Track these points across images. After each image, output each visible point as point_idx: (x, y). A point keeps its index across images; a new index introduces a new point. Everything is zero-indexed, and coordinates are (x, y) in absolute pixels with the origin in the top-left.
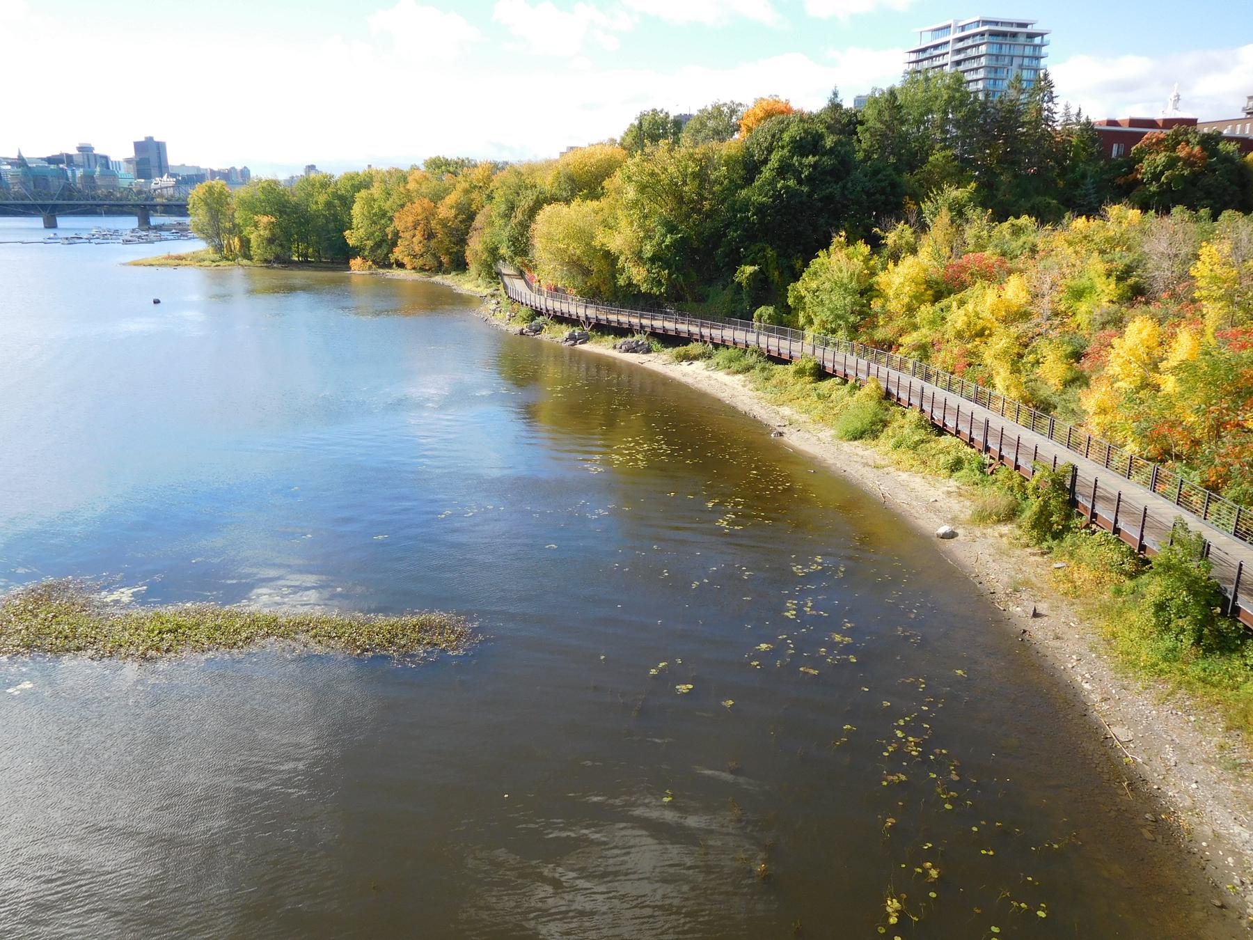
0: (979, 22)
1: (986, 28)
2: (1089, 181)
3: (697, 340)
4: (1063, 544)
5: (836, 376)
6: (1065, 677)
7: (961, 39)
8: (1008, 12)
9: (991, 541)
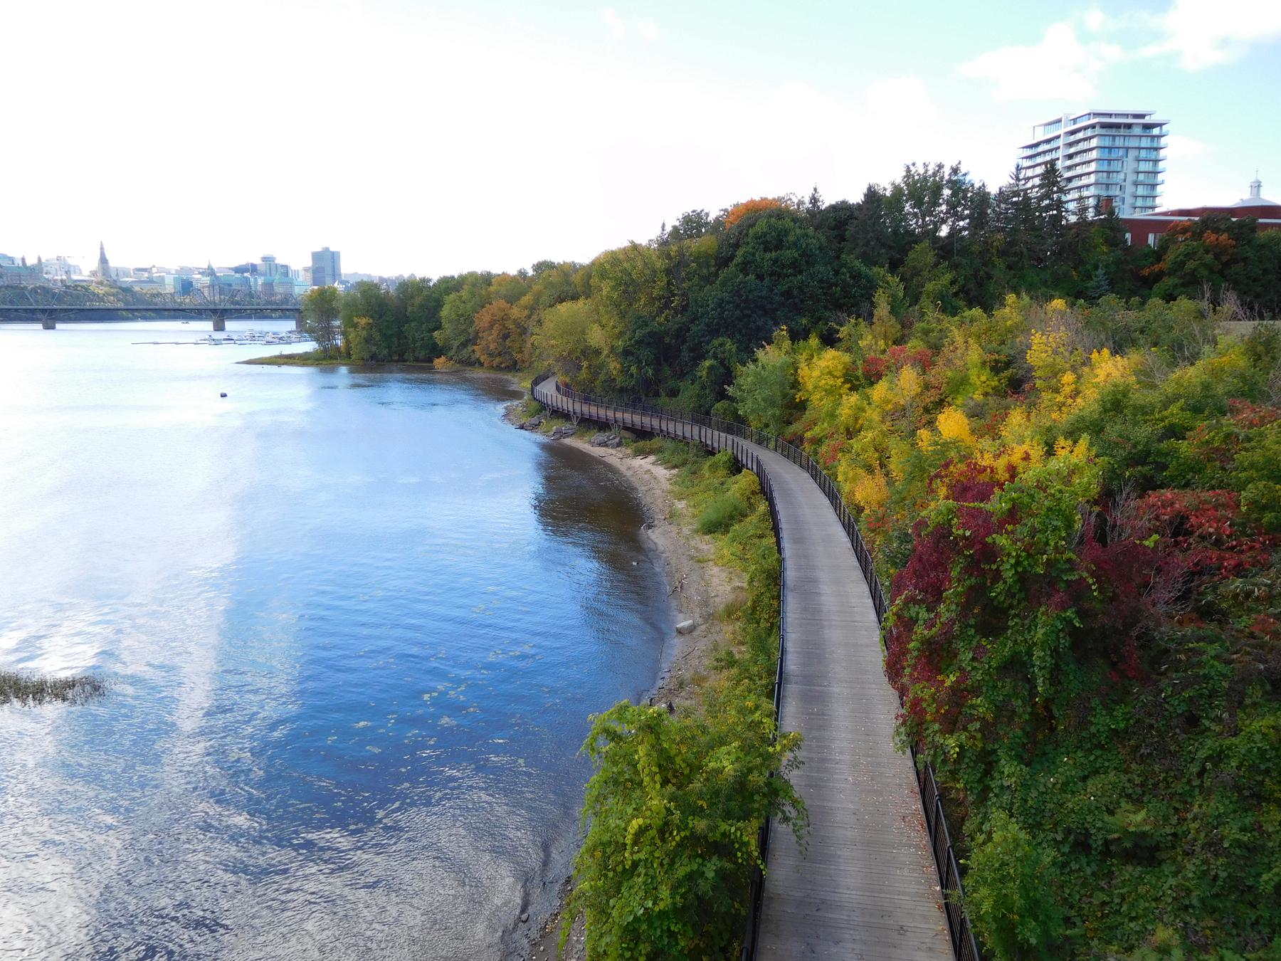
0: (1089, 114)
3: (658, 435)
7: (1073, 133)
8: (1121, 103)
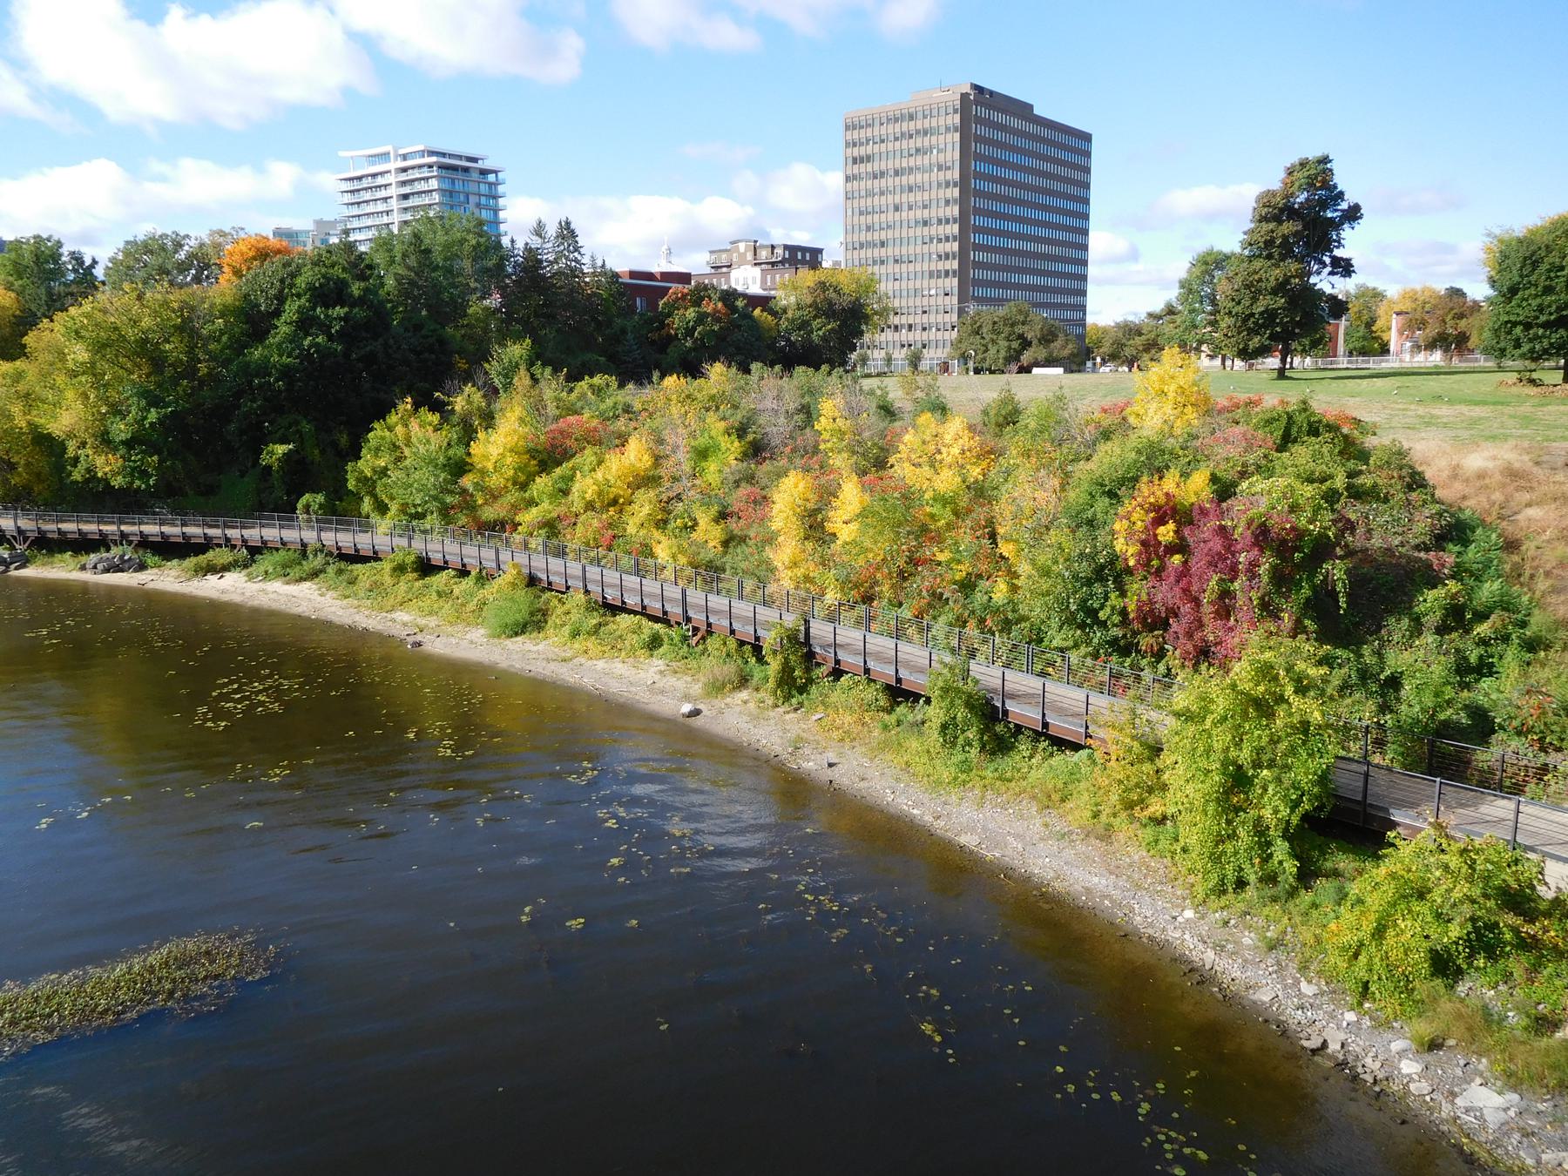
0: (423, 151)
1: (434, 159)
2: (630, 336)
3: (220, 546)
4: (811, 697)
5: (448, 568)
6: (892, 810)
7: (404, 170)
8: (459, 144)
9: (738, 709)
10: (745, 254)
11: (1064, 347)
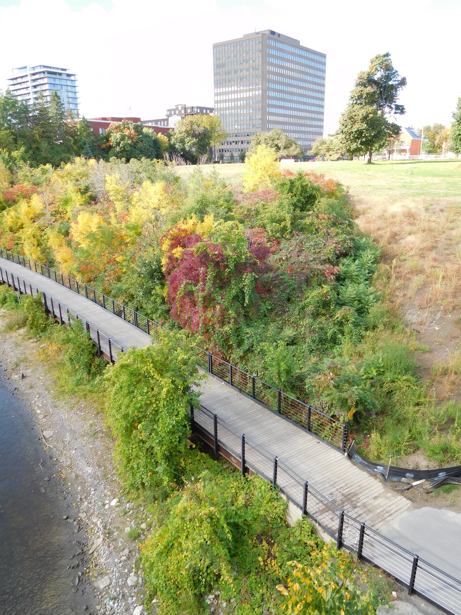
7: (34, 74)
10: (181, 111)
11: (294, 150)
